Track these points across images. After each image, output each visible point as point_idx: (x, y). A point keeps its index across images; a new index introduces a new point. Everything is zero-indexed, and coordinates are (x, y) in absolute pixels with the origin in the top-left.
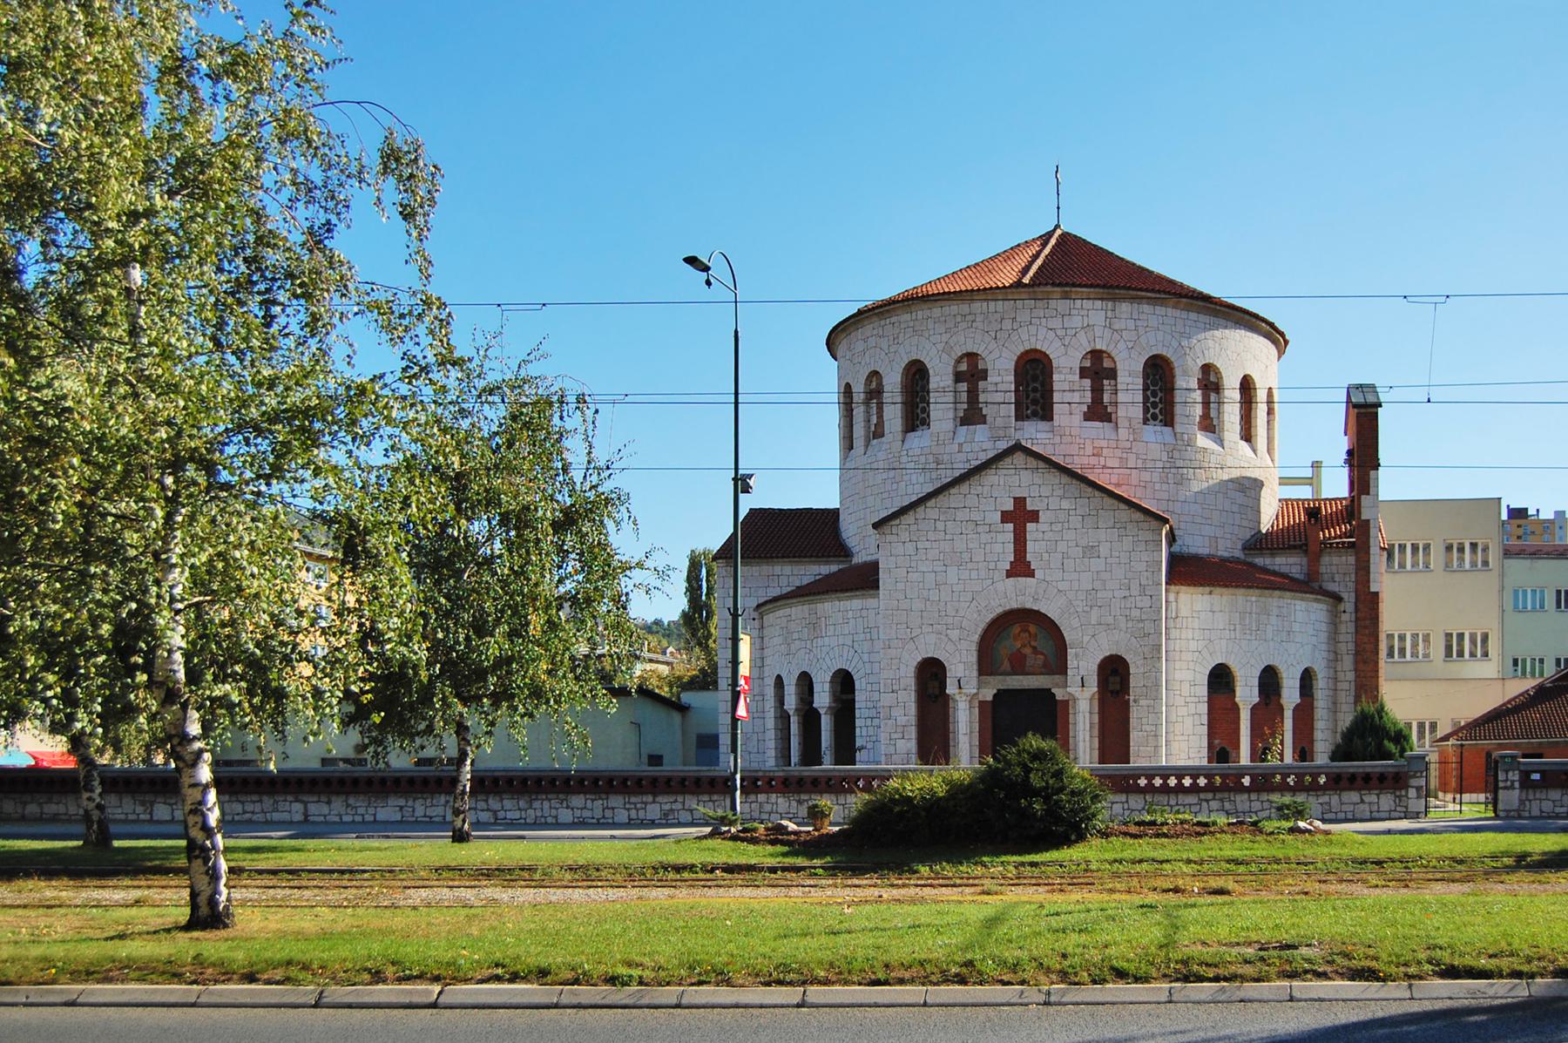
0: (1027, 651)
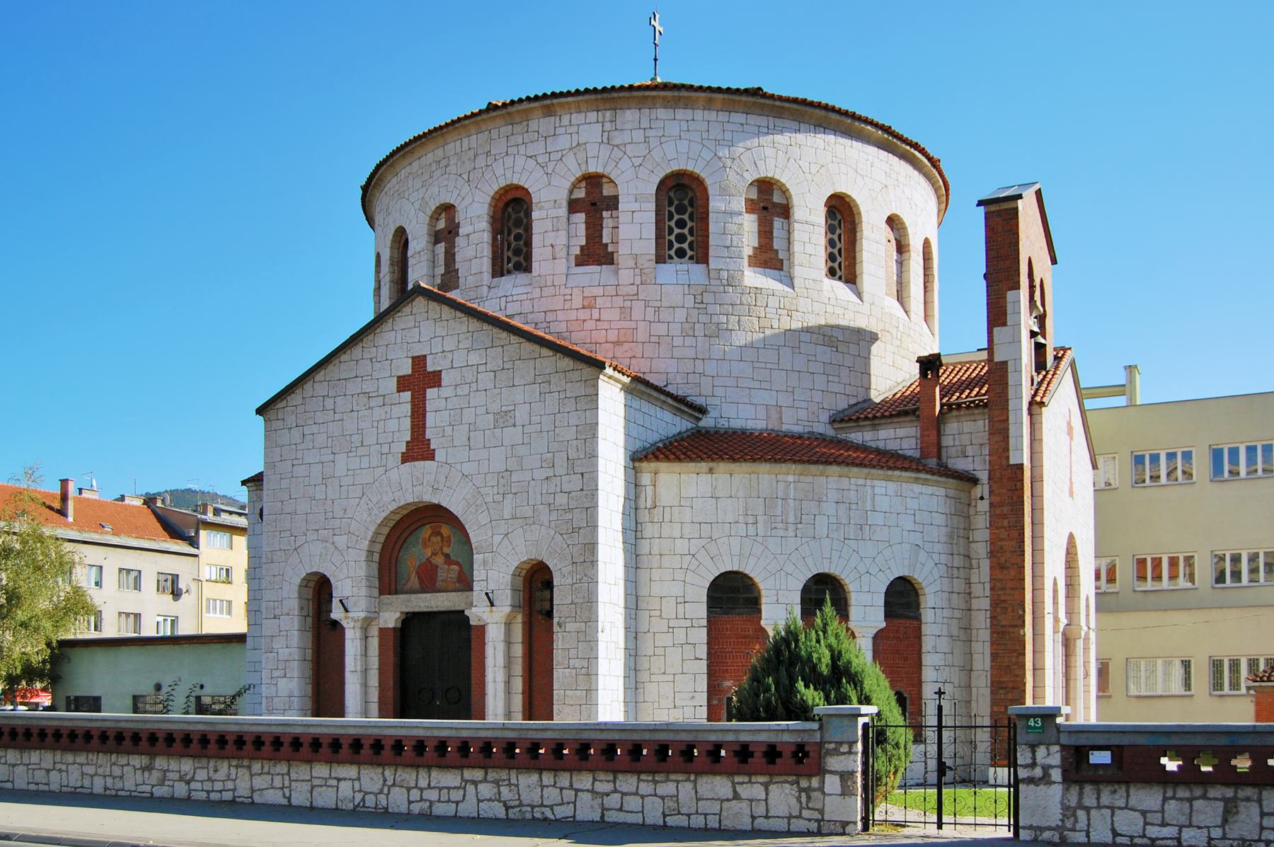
0: (439, 560)
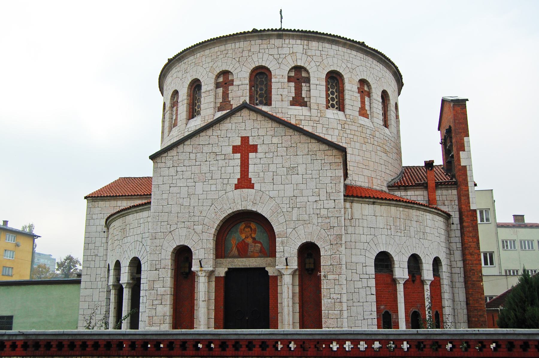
0: (249, 241)
